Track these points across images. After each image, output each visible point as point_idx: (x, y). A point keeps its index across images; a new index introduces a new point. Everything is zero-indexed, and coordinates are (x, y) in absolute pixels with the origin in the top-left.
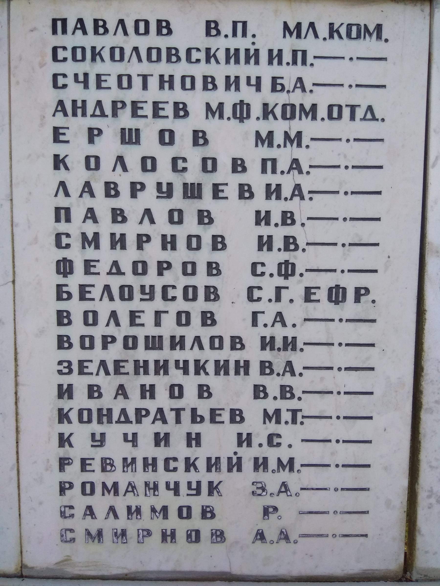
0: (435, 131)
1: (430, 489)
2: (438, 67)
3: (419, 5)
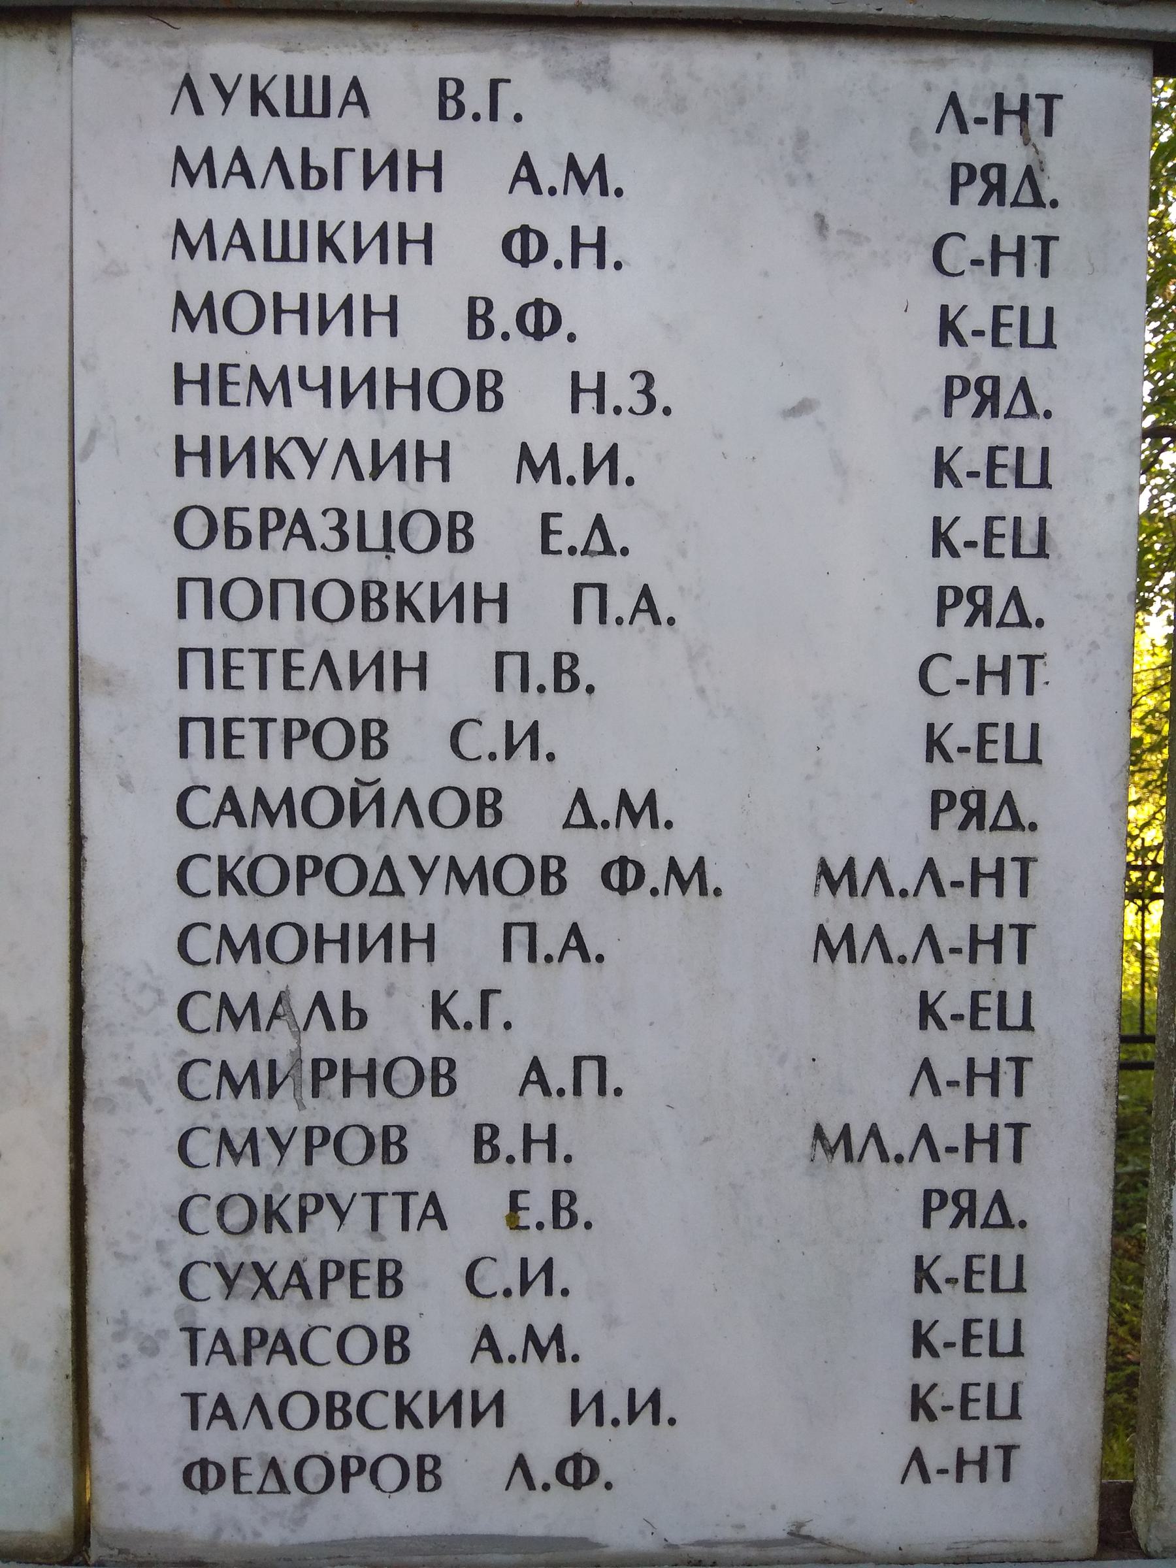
0: (84, 364)
1: (119, 1316)
2: (86, 198)
3: (42, 36)
